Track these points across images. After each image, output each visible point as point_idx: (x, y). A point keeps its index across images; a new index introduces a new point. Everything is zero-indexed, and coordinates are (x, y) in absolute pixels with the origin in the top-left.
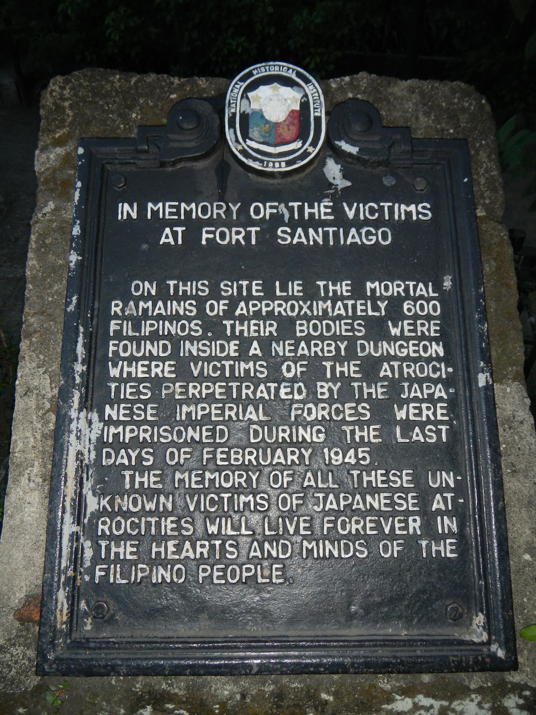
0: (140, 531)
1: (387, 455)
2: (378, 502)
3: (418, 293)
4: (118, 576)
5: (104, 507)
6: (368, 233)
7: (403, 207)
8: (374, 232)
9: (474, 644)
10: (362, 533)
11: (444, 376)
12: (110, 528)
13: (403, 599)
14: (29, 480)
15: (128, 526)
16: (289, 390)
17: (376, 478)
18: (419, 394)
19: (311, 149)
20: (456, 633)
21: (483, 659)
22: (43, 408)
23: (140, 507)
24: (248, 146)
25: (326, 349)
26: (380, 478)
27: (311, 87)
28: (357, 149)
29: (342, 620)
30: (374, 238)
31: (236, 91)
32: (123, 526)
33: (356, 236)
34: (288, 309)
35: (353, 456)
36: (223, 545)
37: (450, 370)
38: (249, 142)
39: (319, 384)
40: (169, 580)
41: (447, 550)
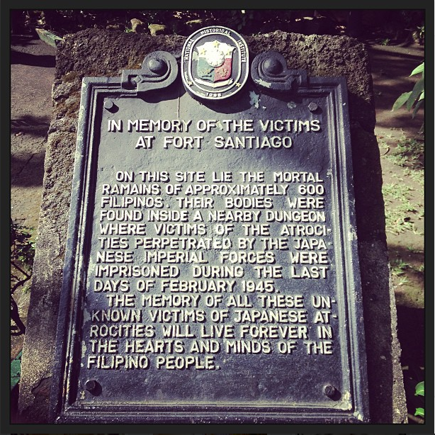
0: (118, 334)
1: (283, 284)
2: (276, 315)
3: (309, 179)
4: (103, 363)
5: (95, 318)
6: (276, 140)
7: (300, 122)
8: (280, 139)
9: (342, 411)
10: (267, 336)
11: (325, 234)
12: (98, 332)
13: (294, 382)
14: (44, 303)
15: (110, 331)
16: (219, 243)
17: (276, 299)
18: (307, 246)
19: (238, 85)
20: (331, 405)
21: (348, 420)
22: (53, 256)
23: (118, 318)
24: (196, 83)
25: (245, 216)
26: (279, 301)
27: (240, 43)
28: (270, 84)
29: (253, 394)
30: (280, 143)
31: (189, 45)
32: (107, 331)
33: (268, 141)
34: (221, 190)
35: (262, 286)
36: (172, 344)
37: (329, 230)
38: (197, 80)
39: (240, 239)
40: (136, 367)
41: (323, 348)
